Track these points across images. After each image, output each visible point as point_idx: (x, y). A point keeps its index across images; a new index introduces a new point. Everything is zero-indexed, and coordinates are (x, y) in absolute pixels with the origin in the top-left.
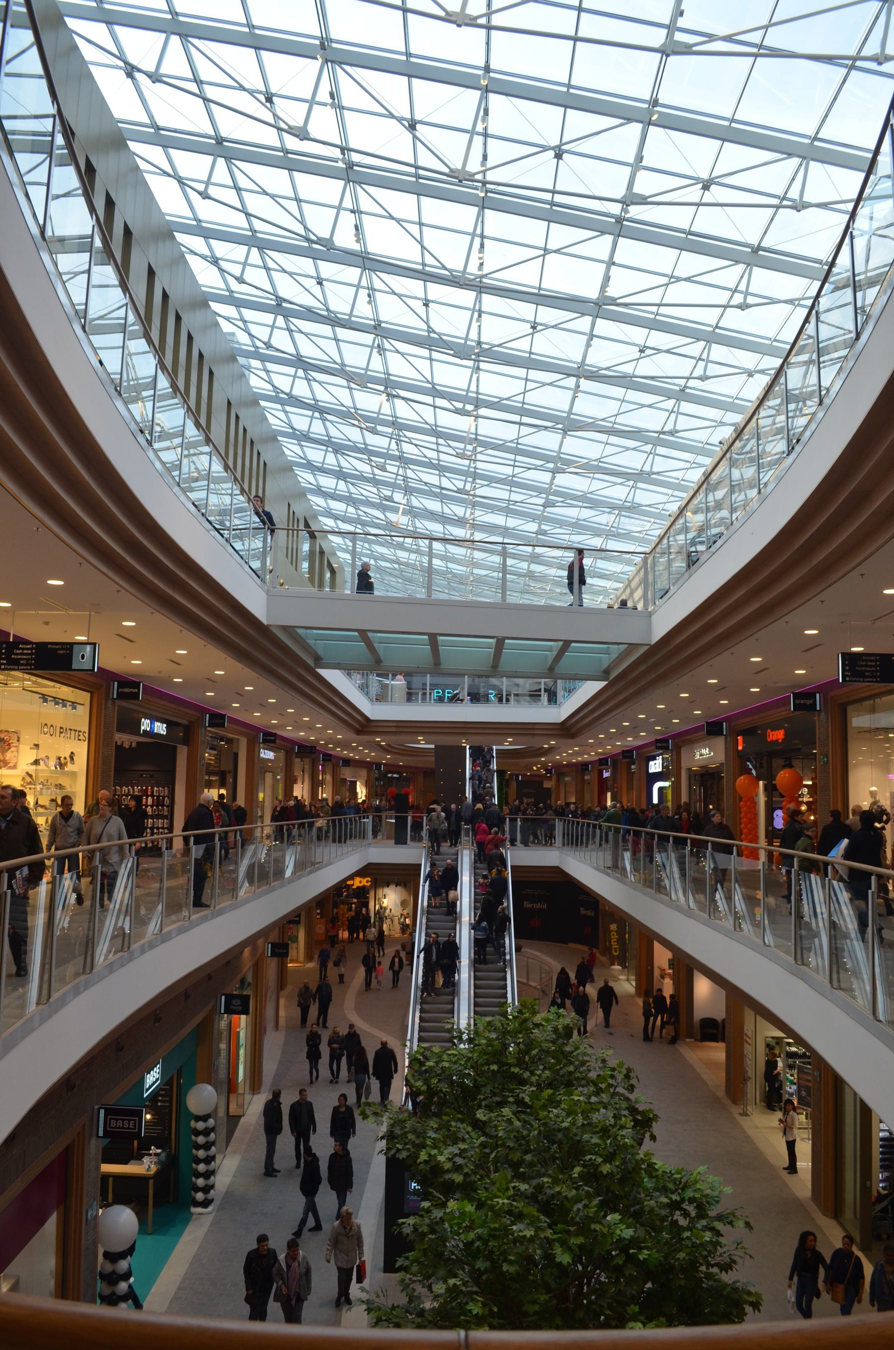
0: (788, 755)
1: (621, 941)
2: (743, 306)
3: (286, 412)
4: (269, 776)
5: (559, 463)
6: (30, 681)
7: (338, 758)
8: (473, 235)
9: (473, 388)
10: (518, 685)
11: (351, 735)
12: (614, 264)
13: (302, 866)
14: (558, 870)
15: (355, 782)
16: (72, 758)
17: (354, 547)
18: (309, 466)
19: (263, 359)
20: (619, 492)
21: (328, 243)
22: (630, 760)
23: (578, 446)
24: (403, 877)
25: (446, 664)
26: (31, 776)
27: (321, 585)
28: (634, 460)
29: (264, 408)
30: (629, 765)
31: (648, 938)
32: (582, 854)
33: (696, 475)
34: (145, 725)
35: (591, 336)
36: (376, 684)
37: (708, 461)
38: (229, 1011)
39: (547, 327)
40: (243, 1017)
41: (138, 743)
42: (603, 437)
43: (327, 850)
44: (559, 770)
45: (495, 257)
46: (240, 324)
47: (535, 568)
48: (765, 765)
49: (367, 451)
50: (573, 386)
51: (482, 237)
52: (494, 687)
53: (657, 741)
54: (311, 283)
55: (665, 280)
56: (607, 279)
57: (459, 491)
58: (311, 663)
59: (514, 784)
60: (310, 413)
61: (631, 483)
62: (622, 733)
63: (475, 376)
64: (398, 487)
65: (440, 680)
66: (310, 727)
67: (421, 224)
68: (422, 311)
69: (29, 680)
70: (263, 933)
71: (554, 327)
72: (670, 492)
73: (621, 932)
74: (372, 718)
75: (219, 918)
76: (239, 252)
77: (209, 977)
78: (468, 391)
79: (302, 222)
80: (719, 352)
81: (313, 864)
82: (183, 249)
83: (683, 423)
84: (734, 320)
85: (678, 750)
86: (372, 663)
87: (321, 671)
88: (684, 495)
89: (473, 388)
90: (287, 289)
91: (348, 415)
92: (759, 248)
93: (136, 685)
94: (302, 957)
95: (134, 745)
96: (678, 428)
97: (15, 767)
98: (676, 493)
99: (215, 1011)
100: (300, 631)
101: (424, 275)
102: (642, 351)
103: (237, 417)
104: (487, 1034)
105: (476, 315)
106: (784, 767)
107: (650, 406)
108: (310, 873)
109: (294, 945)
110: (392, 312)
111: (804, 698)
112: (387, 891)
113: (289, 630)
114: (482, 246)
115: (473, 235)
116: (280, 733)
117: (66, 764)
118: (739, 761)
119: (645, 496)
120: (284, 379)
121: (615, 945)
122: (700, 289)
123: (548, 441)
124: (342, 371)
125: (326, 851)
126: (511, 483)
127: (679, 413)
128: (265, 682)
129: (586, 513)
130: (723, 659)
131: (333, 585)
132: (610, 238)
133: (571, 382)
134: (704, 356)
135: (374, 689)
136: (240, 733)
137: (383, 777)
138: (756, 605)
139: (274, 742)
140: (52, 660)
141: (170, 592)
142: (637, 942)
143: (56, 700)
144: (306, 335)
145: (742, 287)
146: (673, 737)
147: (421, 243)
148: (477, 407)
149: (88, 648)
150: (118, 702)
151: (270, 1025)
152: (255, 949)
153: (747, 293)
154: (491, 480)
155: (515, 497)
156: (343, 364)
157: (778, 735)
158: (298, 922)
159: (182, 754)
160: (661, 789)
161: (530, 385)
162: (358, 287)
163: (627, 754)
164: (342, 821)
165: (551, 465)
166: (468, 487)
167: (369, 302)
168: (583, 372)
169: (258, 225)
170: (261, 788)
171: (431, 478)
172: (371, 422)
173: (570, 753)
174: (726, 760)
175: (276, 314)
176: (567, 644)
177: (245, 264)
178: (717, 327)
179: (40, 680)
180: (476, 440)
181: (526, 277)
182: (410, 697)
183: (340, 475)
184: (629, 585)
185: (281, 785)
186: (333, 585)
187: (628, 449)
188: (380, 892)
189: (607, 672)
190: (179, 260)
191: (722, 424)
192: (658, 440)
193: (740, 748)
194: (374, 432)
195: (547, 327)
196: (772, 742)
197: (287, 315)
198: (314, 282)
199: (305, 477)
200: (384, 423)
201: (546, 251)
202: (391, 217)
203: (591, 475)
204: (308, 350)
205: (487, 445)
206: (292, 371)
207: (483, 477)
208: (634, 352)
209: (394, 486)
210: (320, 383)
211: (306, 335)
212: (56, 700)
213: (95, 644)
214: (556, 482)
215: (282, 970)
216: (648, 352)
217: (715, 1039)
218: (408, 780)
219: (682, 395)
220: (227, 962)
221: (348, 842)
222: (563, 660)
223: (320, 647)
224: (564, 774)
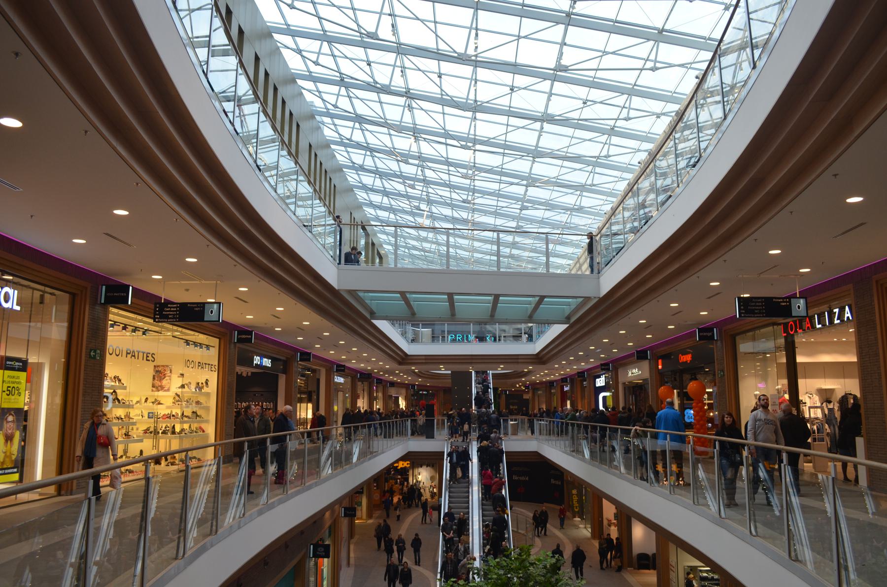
0: (692, 372)
1: (580, 501)
2: (654, 69)
3: (348, 152)
4: (340, 394)
5: (531, 181)
6: (178, 331)
7: (386, 381)
8: (471, 28)
9: (472, 132)
10: (504, 331)
11: (395, 365)
12: (565, 44)
13: (363, 455)
14: (536, 454)
15: (398, 398)
16: (207, 383)
17: (396, 241)
18: (365, 188)
19: (332, 116)
20: (570, 199)
21: (374, 36)
22: (584, 378)
23: (544, 169)
24: (432, 460)
25: (459, 315)
26: (179, 396)
27: (373, 262)
28: (580, 177)
29: (334, 150)
30: (582, 381)
31: (598, 496)
32: (554, 443)
33: (622, 186)
34: (257, 360)
35: (551, 94)
36: (411, 331)
37: (630, 176)
38: (316, 556)
39: (520, 89)
40: (326, 560)
41: (252, 373)
42: (559, 162)
43: (381, 442)
44: (534, 387)
45: (485, 41)
46: (317, 93)
47: (515, 252)
48: (678, 379)
49: (402, 177)
50: (539, 128)
51: (477, 29)
52: (489, 332)
53: (602, 365)
54: (363, 65)
55: (601, 54)
56: (561, 54)
57: (464, 201)
58: (368, 316)
59: (504, 396)
60: (364, 152)
61: (578, 193)
62: (578, 360)
63: (473, 123)
64: (423, 200)
65: (453, 328)
66: (367, 360)
67: (435, 22)
68: (437, 80)
69: (177, 331)
70: (339, 501)
71: (525, 88)
72: (604, 198)
73: (580, 495)
74: (409, 353)
75: (309, 492)
76: (314, 45)
77: (302, 532)
78: (469, 134)
79: (356, 22)
80: (637, 102)
81: (371, 453)
82: (279, 45)
83: (613, 150)
84: (648, 80)
85: (616, 370)
86: (409, 317)
87: (375, 322)
88: (614, 200)
89: (472, 132)
90: (348, 68)
91: (391, 153)
92: (663, 30)
93: (250, 333)
94: (364, 516)
95: (249, 374)
96: (610, 153)
97: (168, 390)
98: (609, 199)
99: (305, 557)
100: (361, 294)
101: (438, 55)
102: (585, 103)
103: (316, 155)
104: (496, 571)
105: (473, 82)
106: (691, 380)
107: (590, 140)
108: (370, 459)
109: (359, 508)
110: (418, 82)
111: (706, 331)
112: (420, 470)
113: (353, 293)
114: (477, 35)
115: (471, 28)
116: (347, 365)
117: (203, 387)
118: (661, 378)
119: (588, 201)
120: (346, 129)
121: (576, 504)
122: (624, 59)
123: (522, 166)
124: (385, 124)
125: (379, 443)
126: (498, 195)
127: (610, 144)
128: (338, 330)
129: (548, 214)
130: (652, 306)
131: (381, 262)
132: (562, 27)
133: (537, 125)
134: (627, 105)
135: (410, 336)
136: (321, 366)
137: (416, 393)
138: (676, 266)
139: (343, 371)
140: (190, 315)
141: (271, 266)
142: (590, 500)
143: (195, 344)
144: (361, 100)
145: (652, 57)
146: (613, 362)
147: (435, 33)
148: (474, 144)
149: (215, 306)
150: (238, 345)
151: (344, 563)
152: (333, 512)
153: (656, 61)
154: (484, 193)
155: (500, 204)
156: (385, 119)
157: (688, 358)
158: (362, 493)
159: (282, 381)
160: (604, 398)
161: (510, 129)
162: (394, 66)
163: (581, 374)
164: (387, 423)
165: (525, 182)
166: (470, 198)
167: (402, 76)
168: (547, 118)
169: (328, 26)
170: (335, 402)
171: (445, 193)
172: (404, 157)
173: (542, 375)
174: (651, 376)
175: (341, 86)
176: (542, 298)
177: (319, 53)
178: (635, 85)
179: (184, 330)
180: (475, 167)
181: (506, 55)
182: (434, 338)
183: (385, 193)
184: (578, 261)
185: (349, 400)
186: (381, 262)
187: (575, 170)
188: (416, 471)
189: (568, 318)
190: (276, 52)
191: (639, 150)
192: (596, 163)
193: (660, 367)
194: (407, 163)
195: (520, 89)
196: (683, 363)
197: (347, 86)
198: (365, 64)
199: (361, 195)
200: (413, 157)
201: (519, 37)
202: (418, 19)
203: (551, 188)
204: (362, 109)
205: (481, 170)
206: (351, 124)
207: (479, 192)
208: (580, 104)
209: (420, 199)
210: (371, 132)
211: (361, 100)
212: (195, 344)
213: (220, 303)
214: (528, 193)
215: (352, 525)
216: (589, 103)
217: (647, 567)
218: (433, 395)
219: (612, 132)
220: (315, 521)
221: (395, 438)
222: (538, 311)
223: (373, 305)
224: (538, 389)
